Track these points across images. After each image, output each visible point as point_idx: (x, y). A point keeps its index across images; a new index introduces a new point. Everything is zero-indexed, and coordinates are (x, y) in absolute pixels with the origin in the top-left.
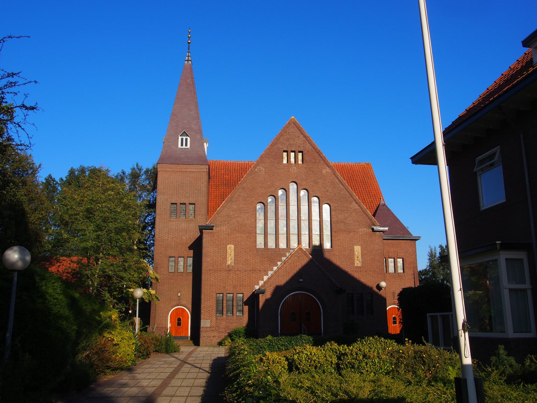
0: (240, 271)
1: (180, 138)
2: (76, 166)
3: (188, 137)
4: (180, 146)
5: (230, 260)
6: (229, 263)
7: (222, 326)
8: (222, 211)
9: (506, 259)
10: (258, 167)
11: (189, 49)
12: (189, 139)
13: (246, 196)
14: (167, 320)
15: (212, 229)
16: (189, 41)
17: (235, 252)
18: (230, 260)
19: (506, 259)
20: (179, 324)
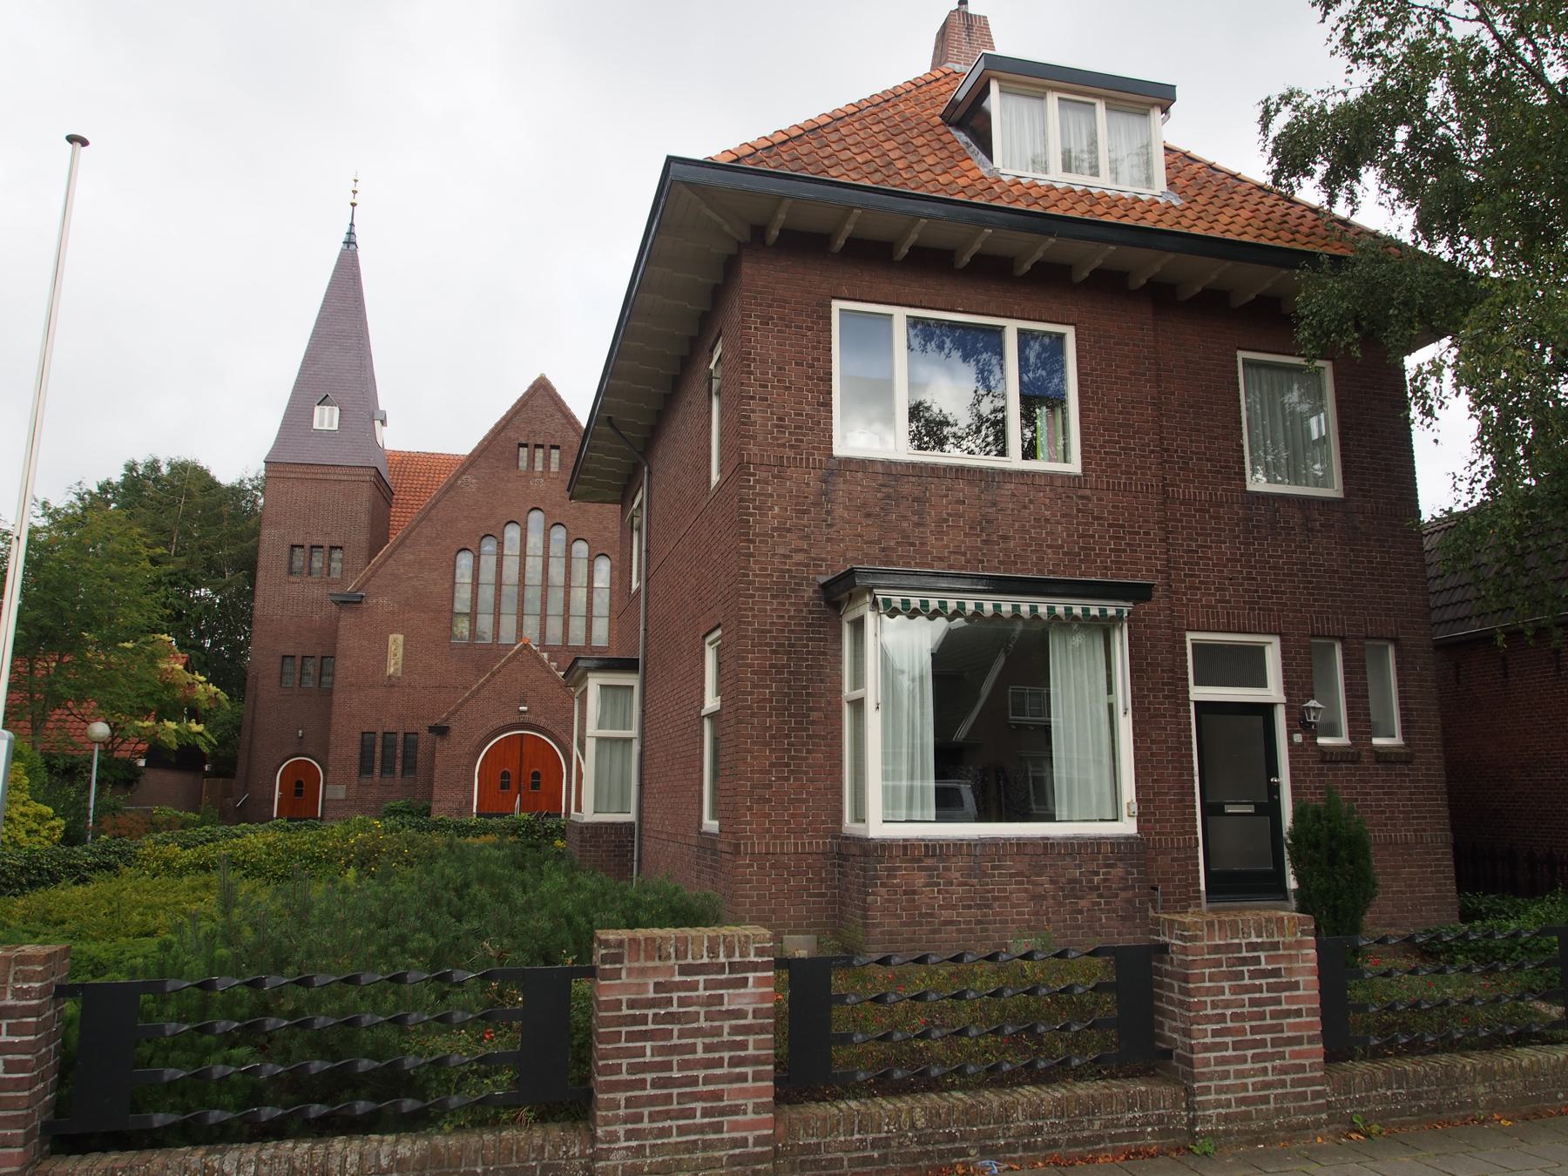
5: (394, 666)
10: (464, 477)
18: (394, 666)
20: (299, 793)
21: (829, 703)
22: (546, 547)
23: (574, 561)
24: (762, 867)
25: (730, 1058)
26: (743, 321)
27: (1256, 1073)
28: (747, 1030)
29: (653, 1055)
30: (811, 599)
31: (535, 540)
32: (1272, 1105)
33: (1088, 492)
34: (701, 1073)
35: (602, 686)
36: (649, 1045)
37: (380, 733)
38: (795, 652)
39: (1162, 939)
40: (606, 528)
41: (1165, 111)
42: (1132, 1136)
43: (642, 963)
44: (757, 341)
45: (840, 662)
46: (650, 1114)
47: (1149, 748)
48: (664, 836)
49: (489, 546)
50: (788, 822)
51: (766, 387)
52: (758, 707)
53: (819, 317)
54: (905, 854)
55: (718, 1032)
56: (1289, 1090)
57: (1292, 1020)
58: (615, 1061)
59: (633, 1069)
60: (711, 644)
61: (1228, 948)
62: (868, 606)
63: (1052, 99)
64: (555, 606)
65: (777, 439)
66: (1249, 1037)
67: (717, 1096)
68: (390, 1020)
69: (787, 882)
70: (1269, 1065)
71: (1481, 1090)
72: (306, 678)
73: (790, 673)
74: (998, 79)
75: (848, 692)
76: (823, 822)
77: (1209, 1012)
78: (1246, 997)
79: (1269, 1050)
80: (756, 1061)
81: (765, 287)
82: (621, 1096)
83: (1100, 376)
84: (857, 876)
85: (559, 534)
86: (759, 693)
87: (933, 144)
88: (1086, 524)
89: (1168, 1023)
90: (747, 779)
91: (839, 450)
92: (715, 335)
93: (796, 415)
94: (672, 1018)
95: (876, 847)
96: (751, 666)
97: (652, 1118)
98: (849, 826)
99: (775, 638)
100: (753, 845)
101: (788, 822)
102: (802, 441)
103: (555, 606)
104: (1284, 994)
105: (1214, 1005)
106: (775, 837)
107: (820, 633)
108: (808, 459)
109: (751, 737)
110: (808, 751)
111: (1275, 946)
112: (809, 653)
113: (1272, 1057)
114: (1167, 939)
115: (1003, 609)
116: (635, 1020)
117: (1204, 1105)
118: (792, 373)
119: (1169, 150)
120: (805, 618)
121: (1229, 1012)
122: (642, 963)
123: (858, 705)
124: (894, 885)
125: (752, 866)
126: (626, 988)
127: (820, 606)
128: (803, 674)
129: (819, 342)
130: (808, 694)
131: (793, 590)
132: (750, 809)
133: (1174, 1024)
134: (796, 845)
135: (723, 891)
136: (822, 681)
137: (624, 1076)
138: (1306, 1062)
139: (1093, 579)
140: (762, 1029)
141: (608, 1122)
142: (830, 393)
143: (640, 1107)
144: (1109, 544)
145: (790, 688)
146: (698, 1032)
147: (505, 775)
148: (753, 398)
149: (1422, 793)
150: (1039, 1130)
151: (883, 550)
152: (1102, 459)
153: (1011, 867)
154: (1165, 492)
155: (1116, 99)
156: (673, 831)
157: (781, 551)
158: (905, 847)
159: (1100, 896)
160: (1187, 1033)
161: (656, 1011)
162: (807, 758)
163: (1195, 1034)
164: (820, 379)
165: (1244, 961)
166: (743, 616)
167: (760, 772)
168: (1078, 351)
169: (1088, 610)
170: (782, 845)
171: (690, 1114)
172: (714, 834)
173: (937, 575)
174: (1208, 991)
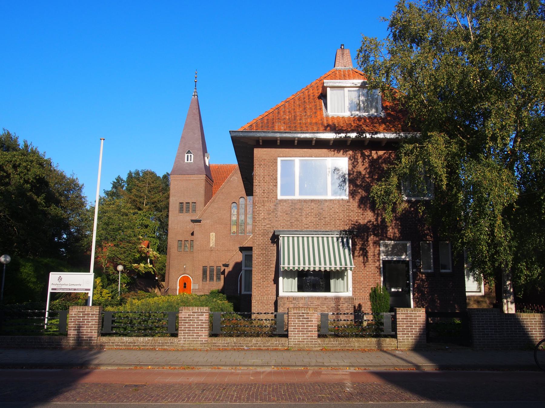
0: (219, 251)
1: (186, 155)
2: (133, 171)
3: (191, 154)
4: (186, 161)
5: (212, 244)
6: (211, 245)
7: (206, 288)
8: (207, 209)
10: (233, 177)
11: (196, 86)
12: (192, 156)
13: (224, 198)
14: (176, 284)
15: (200, 222)
16: (196, 81)
17: (215, 238)
18: (212, 244)
20: (185, 287)
24: (258, 303)
27: (302, 336)
28: (204, 323)
32: (305, 343)
34: (195, 329)
35: (245, 255)
36: (187, 324)
37: (208, 267)
42: (276, 346)
43: (186, 311)
47: (366, 273)
50: (265, 292)
52: (258, 264)
53: (274, 163)
54: (288, 300)
55: (198, 323)
56: (309, 340)
57: (311, 327)
61: (297, 313)
67: (198, 333)
70: (305, 335)
71: (357, 344)
73: (266, 255)
77: (293, 325)
78: (301, 322)
80: (205, 328)
82: (182, 332)
93: (268, 189)
94: (191, 320)
96: (256, 253)
97: (187, 336)
99: (262, 246)
101: (265, 292)
102: (269, 196)
104: (309, 322)
106: (262, 296)
110: (270, 275)
111: (308, 313)
112: (271, 250)
116: (185, 320)
117: (290, 342)
118: (267, 178)
122: (186, 311)
124: (285, 307)
126: (183, 315)
128: (269, 255)
129: (274, 169)
130: (270, 260)
131: (267, 234)
132: (255, 289)
134: (267, 298)
137: (183, 329)
138: (314, 335)
140: (206, 323)
141: (180, 336)
142: (277, 183)
145: (266, 259)
146: (195, 323)
150: (258, 344)
151: (291, 223)
153: (316, 303)
157: (264, 224)
158: (288, 298)
164: (274, 179)
165: (301, 316)
166: (254, 241)
167: (258, 280)
171: (194, 336)
173: (296, 231)
174: (292, 321)
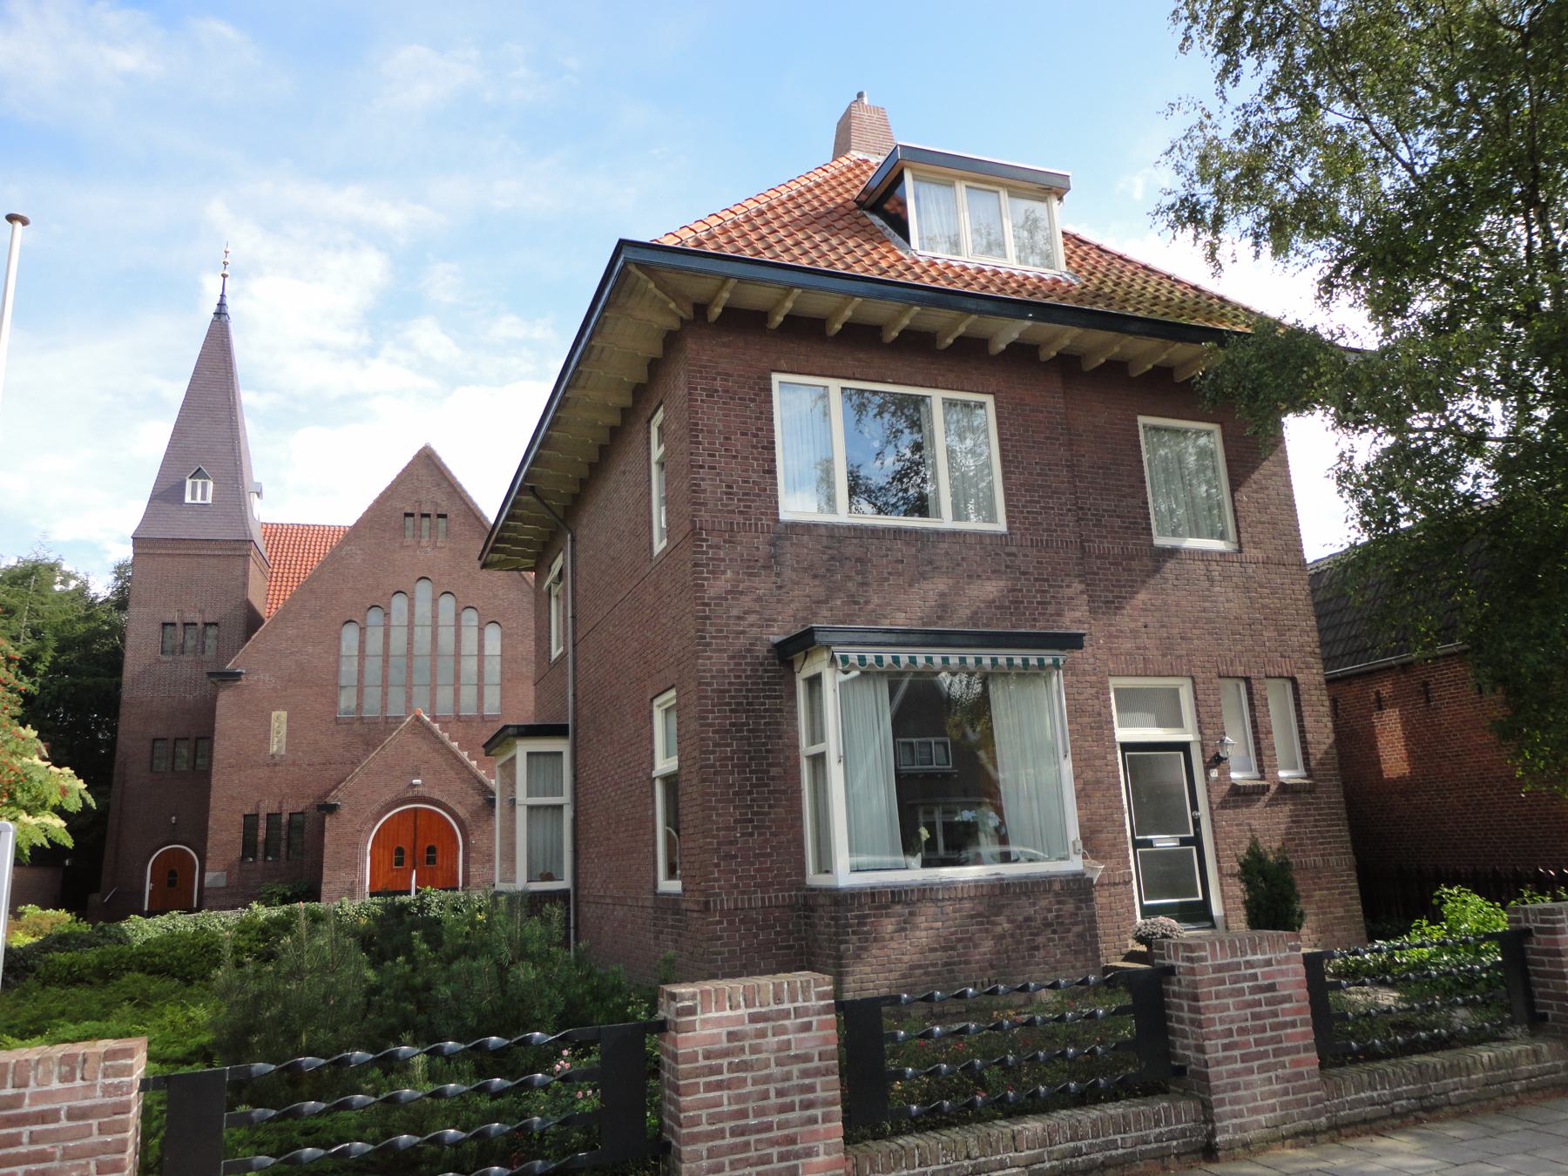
6: (274, 749)
9: (529, 754)
19: (529, 754)
20: (172, 884)
21: (788, 758)
22: (435, 616)
23: (463, 629)
24: (731, 923)
25: (801, 1102)
26: (690, 394)
29: (730, 1104)
30: (766, 658)
31: (423, 608)
33: (1014, 549)
38: (753, 711)
39: (1167, 962)
40: (495, 596)
41: (1060, 199)
44: (703, 413)
45: (796, 718)
46: (731, 1163)
48: (609, 901)
49: (375, 617)
50: (754, 877)
51: (714, 456)
52: (721, 766)
54: (873, 901)
58: (696, 1113)
59: (713, 1119)
60: (659, 706)
62: (826, 663)
63: (961, 188)
64: (446, 675)
65: (727, 505)
66: (1254, 1049)
68: (474, 1090)
69: (756, 936)
72: (178, 761)
74: (912, 169)
75: (806, 749)
76: (789, 875)
79: (1272, 1060)
81: (709, 361)
83: (1018, 441)
84: (828, 926)
85: (447, 604)
86: (721, 752)
87: (852, 226)
88: (1015, 579)
89: (1179, 1041)
90: (713, 837)
91: (785, 516)
92: (655, 404)
94: (744, 1066)
95: (845, 895)
98: (814, 879)
100: (722, 901)
102: (750, 507)
103: (446, 675)
105: (1222, 1021)
106: (743, 893)
107: (775, 691)
108: (756, 525)
109: (715, 795)
110: (770, 806)
113: (1274, 1067)
114: (1173, 962)
115: (951, 661)
118: (738, 442)
119: (1064, 234)
120: (761, 677)
121: (1234, 1027)
123: (819, 760)
125: (722, 923)
127: (774, 664)
130: (768, 751)
132: (717, 865)
133: (1186, 1041)
134: (763, 899)
135: (691, 950)
136: (780, 737)
139: (1023, 630)
140: (828, 1072)
142: (774, 460)
143: (721, 1156)
144: (1035, 597)
147: (400, 851)
148: (701, 467)
149: (1324, 820)
152: (1026, 518)
154: (1083, 548)
155: (1015, 187)
156: (621, 894)
158: (873, 894)
159: (1054, 932)
160: (1201, 1049)
161: (730, 1059)
162: (769, 813)
163: (1208, 1049)
164: (763, 448)
166: (702, 677)
168: (998, 418)
169: (1012, 659)
170: (750, 899)
172: (678, 895)
